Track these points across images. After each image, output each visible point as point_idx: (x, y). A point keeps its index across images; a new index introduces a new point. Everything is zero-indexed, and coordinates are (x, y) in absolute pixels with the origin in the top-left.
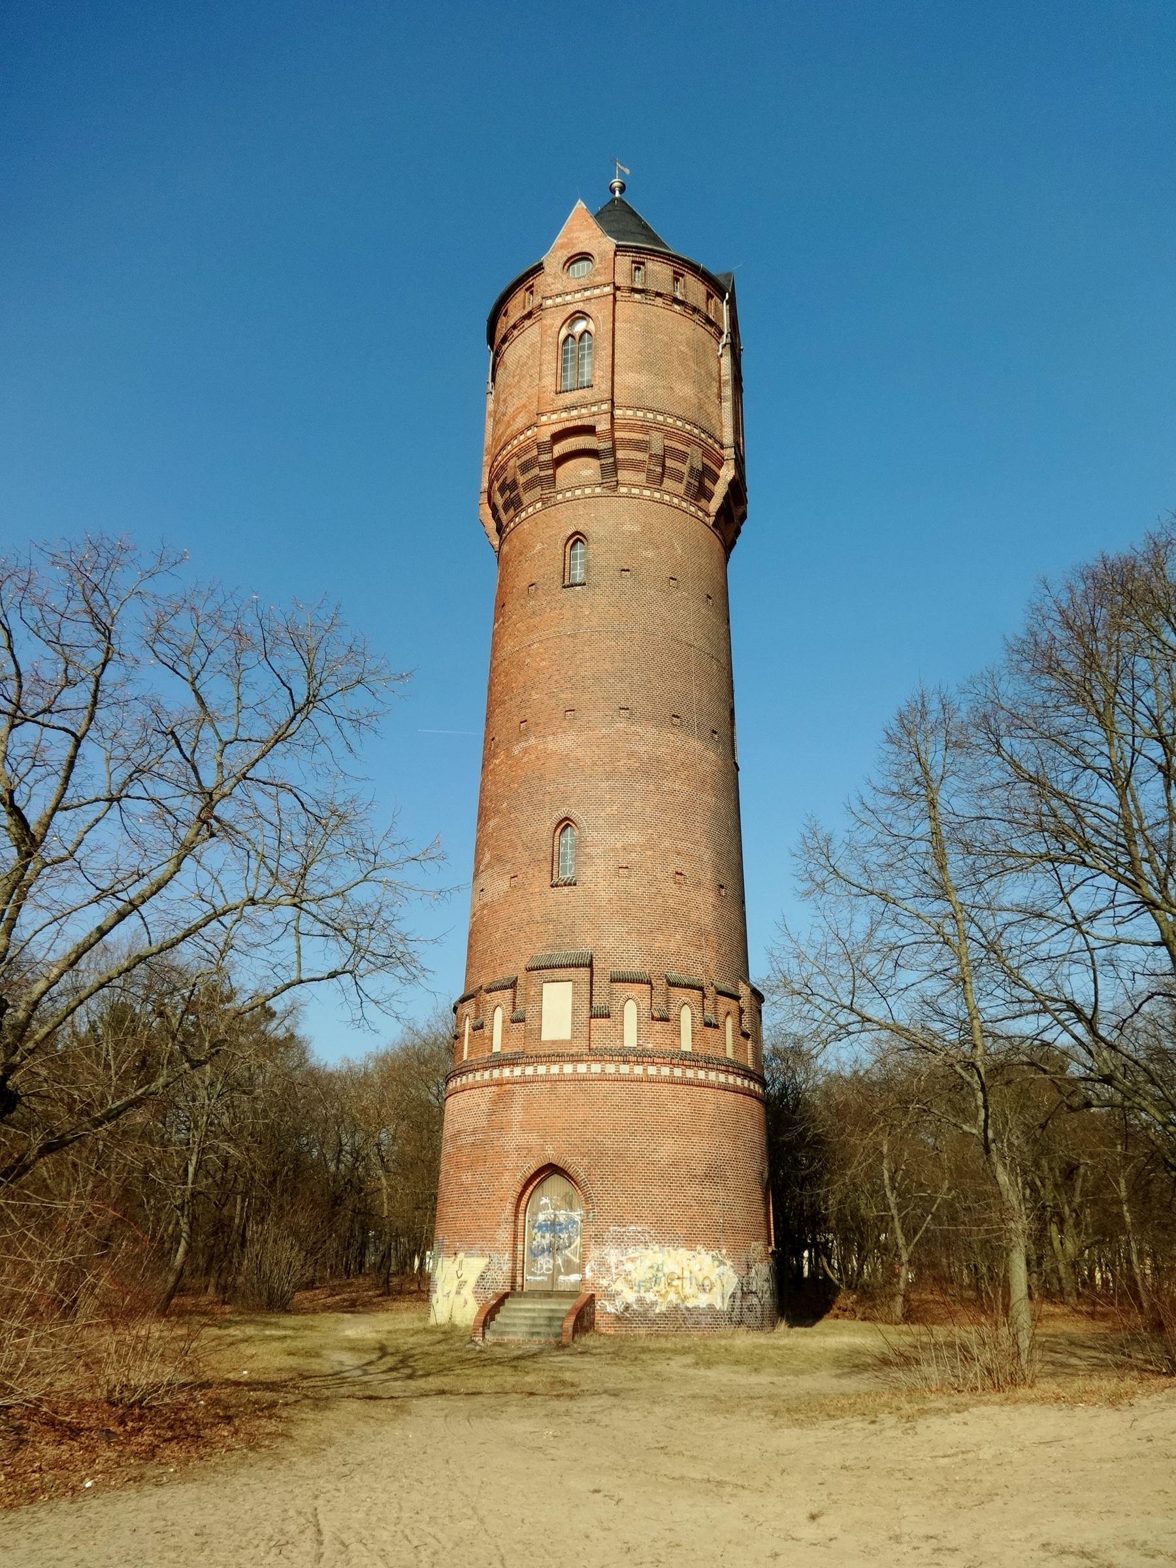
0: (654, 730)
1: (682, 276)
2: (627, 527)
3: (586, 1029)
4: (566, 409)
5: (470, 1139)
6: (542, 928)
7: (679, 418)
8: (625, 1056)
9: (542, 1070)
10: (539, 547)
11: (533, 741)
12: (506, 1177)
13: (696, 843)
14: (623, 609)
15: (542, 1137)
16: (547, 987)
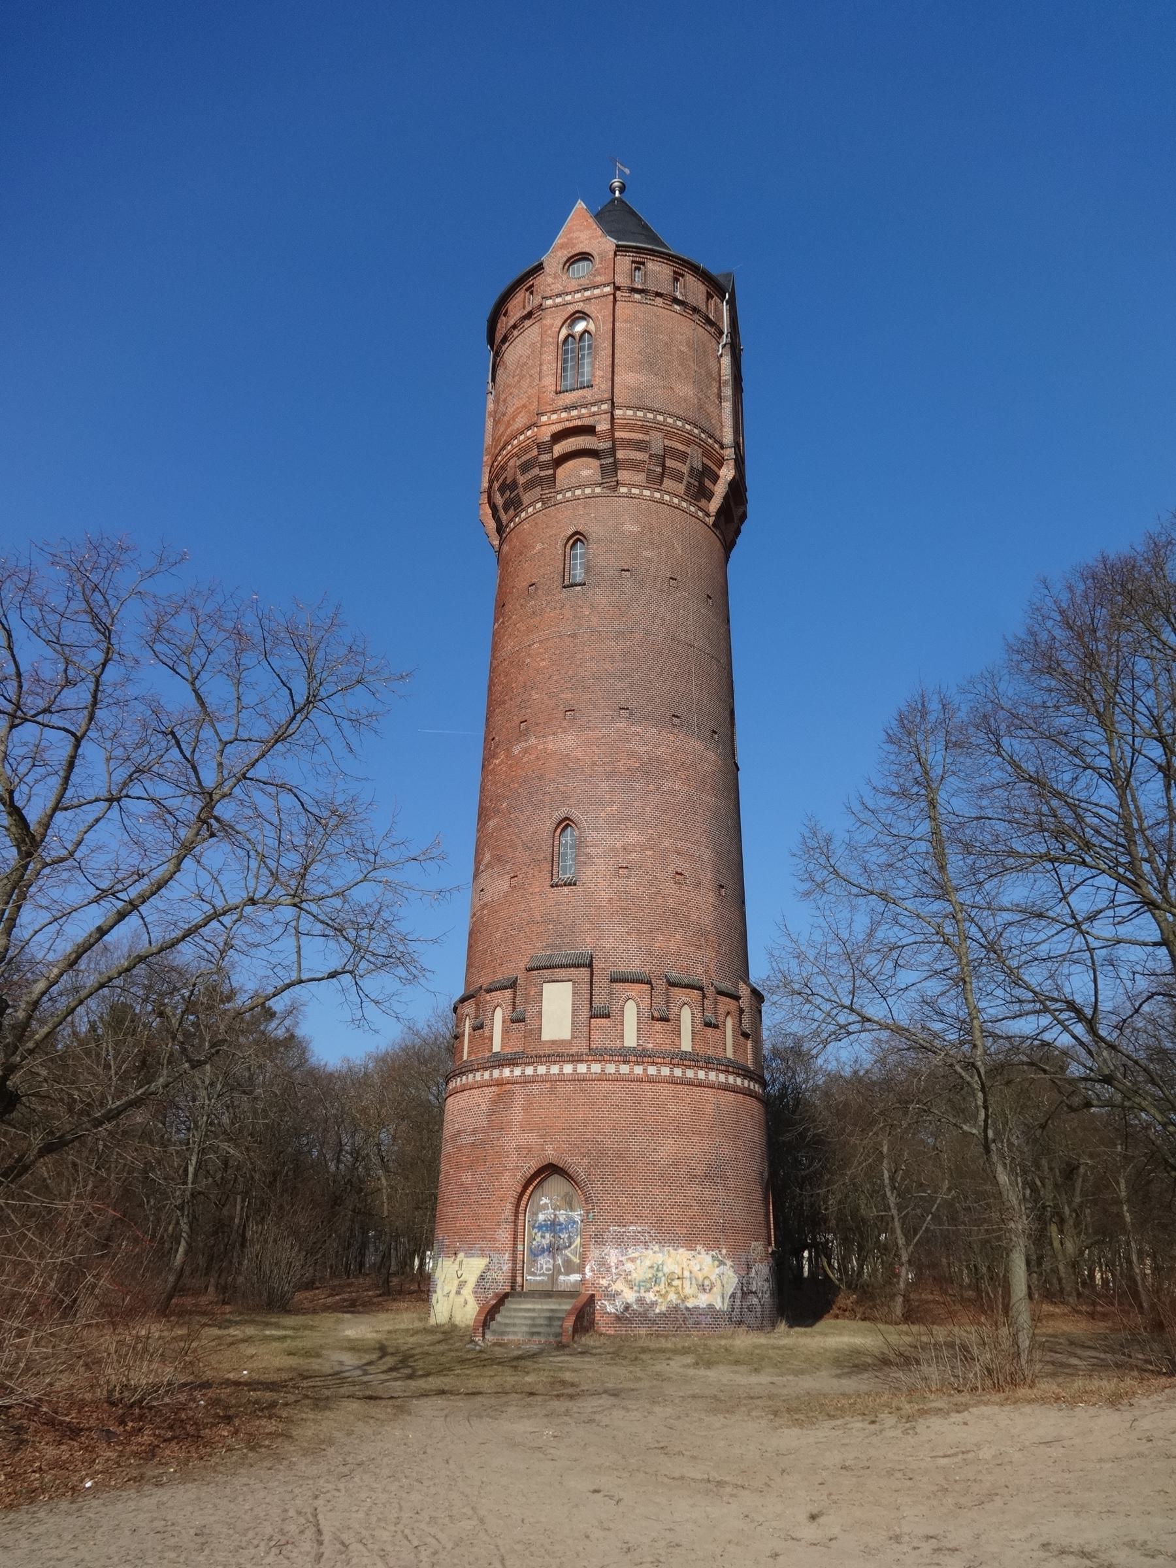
0: (654, 730)
1: (683, 276)
2: (627, 527)
3: (586, 1029)
4: (567, 409)
6: (542, 928)
7: (679, 418)
8: (625, 1055)
9: (542, 1070)
10: (539, 547)
11: (533, 741)
12: (506, 1177)
13: (696, 843)
14: (623, 609)
16: (547, 987)
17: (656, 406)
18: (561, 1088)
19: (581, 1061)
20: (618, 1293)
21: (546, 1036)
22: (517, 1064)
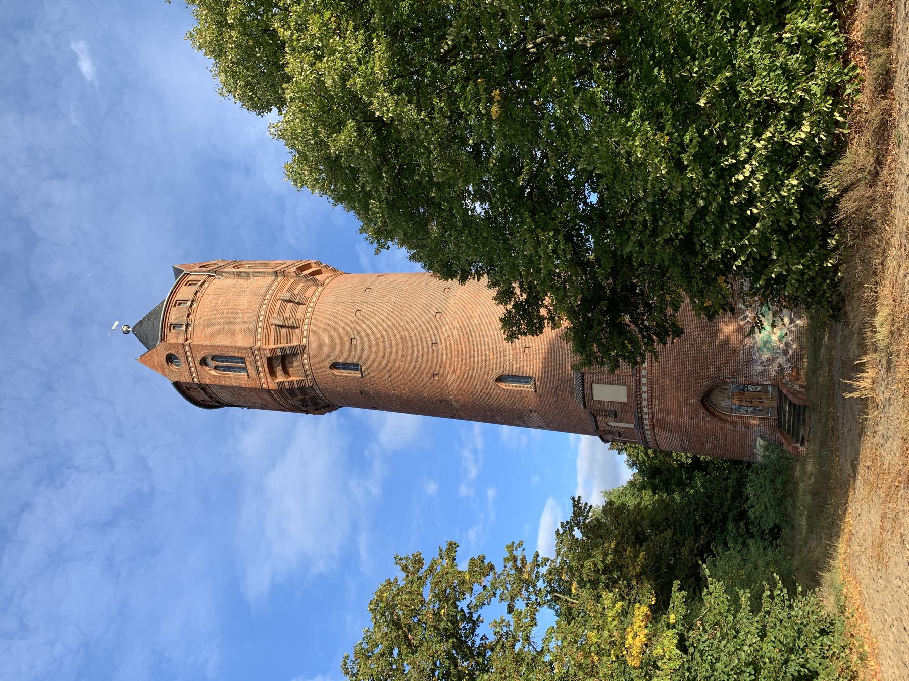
4: (258, 373)
5: (686, 443)
6: (561, 398)
9: (645, 403)
12: (709, 426)
15: (685, 405)
16: (595, 398)
17: (254, 320)
18: (656, 392)
19: (640, 381)
20: (780, 366)
21: (624, 399)
22: (642, 416)
